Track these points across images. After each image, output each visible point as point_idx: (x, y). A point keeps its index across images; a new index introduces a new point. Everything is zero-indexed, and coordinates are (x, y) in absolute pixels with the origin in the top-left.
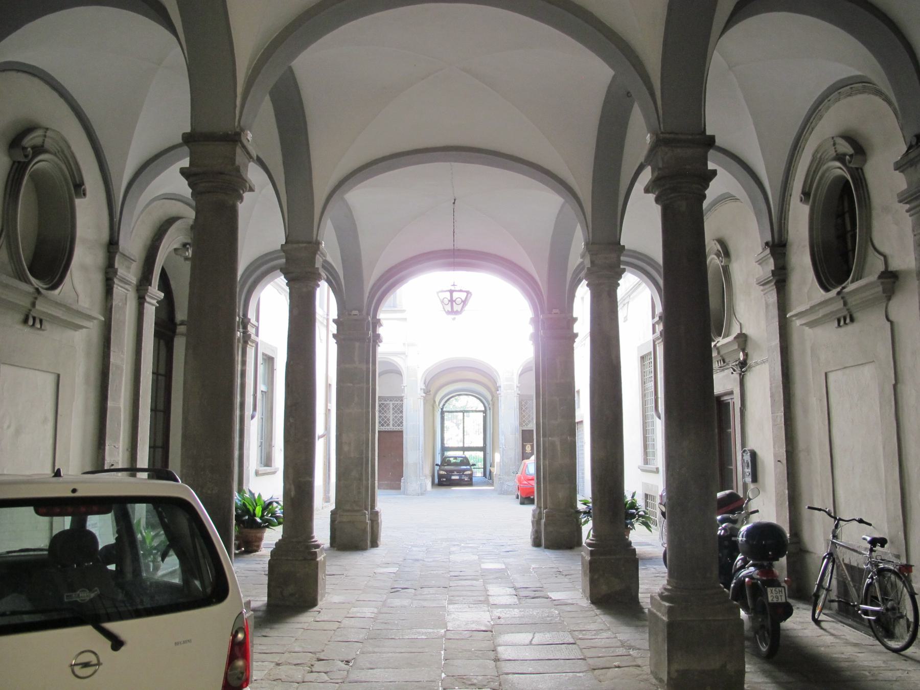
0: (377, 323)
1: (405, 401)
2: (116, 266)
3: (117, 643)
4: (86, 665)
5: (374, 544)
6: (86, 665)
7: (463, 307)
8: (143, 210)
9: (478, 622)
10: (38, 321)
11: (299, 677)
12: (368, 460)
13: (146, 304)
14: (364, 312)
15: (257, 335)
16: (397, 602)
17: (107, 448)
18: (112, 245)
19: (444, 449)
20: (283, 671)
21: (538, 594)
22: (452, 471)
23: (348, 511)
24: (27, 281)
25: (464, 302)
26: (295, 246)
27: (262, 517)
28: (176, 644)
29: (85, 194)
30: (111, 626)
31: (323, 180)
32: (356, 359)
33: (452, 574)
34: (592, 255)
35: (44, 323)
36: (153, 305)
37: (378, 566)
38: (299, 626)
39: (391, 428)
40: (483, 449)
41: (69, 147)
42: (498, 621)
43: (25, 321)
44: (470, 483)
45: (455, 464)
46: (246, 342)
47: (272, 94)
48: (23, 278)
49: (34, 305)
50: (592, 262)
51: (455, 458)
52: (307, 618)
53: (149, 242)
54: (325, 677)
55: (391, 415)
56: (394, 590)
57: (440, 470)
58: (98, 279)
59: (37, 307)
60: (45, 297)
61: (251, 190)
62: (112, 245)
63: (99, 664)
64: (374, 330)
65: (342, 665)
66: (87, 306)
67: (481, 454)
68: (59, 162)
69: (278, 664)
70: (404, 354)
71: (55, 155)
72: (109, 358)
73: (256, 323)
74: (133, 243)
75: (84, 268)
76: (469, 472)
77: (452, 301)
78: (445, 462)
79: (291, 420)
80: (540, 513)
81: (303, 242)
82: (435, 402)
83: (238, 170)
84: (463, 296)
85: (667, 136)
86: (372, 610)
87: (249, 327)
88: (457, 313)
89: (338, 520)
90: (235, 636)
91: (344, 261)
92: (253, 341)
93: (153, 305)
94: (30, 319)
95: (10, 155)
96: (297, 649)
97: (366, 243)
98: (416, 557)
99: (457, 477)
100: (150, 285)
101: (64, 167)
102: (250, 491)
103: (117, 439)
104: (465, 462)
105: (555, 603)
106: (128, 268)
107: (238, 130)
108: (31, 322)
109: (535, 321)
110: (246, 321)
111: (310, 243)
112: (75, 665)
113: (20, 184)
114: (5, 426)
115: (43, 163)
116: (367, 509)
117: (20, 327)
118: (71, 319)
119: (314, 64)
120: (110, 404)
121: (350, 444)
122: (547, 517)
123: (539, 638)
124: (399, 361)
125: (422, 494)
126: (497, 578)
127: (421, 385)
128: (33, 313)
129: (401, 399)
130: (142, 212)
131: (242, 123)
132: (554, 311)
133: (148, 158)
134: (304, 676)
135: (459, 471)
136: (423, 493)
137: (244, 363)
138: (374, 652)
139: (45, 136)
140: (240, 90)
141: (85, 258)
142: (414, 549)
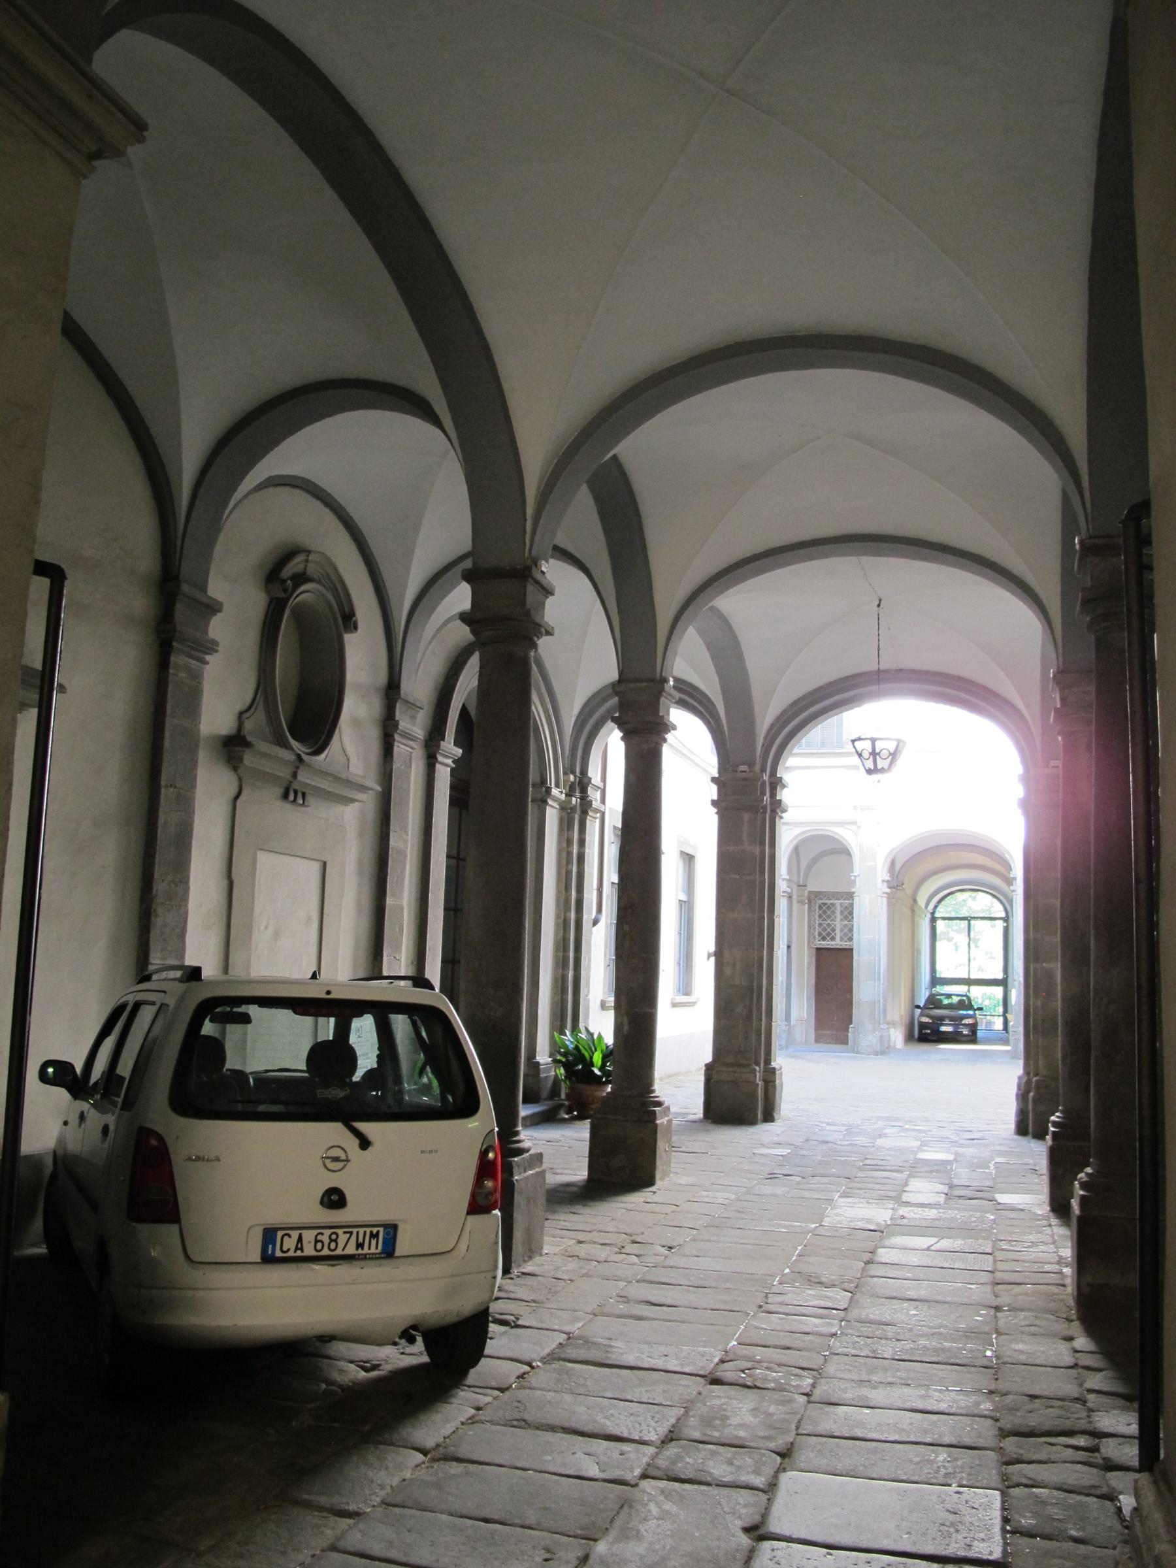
0: (776, 783)
1: (856, 900)
2: (398, 716)
3: (365, 1143)
4: (336, 1159)
5: (769, 1117)
6: (336, 1159)
7: (890, 765)
8: (433, 638)
9: (869, 1221)
10: (300, 795)
11: (603, 1257)
12: (760, 989)
13: (438, 766)
14: (757, 767)
15: (603, 801)
16: (768, 1189)
17: (385, 959)
18: (392, 690)
19: (935, 981)
20: (582, 1251)
21: (979, 1194)
22: (940, 1020)
23: (731, 1065)
24: (288, 747)
25: (894, 756)
26: (632, 685)
27: (602, 1068)
28: (423, 1152)
29: (356, 628)
30: (362, 1126)
31: (669, 587)
32: (745, 838)
33: (868, 1162)
34: (1062, 689)
35: (308, 797)
36: (447, 765)
37: (763, 1145)
38: (622, 1205)
39: (837, 943)
40: (1003, 983)
41: (336, 569)
42: (898, 1222)
43: (285, 796)
44: (972, 1038)
45: (950, 1007)
46: (584, 813)
47: (591, 484)
48: (282, 743)
49: (295, 775)
50: (1063, 700)
51: (949, 996)
52: (635, 1199)
53: (441, 680)
54: (635, 1259)
55: (838, 923)
56: (772, 1176)
57: (922, 1015)
58: (373, 735)
59: (299, 778)
60: (309, 766)
61: (549, 633)
62: (392, 690)
63: (348, 1161)
64: (773, 795)
65: (664, 1251)
66: (360, 772)
67: (998, 991)
68: (325, 592)
69: (580, 1242)
70: (855, 823)
71: (319, 582)
72: (388, 839)
73: (601, 785)
74: (419, 684)
75: (356, 723)
76: (969, 1021)
77: (874, 754)
78: (933, 1002)
79: (626, 928)
80: (1028, 1082)
81: (643, 681)
82: (915, 901)
83: (528, 614)
84: (891, 747)
85: (1096, 541)
86: (726, 1195)
87: (590, 791)
88: (882, 770)
89: (715, 1077)
90: (484, 1154)
91: (725, 691)
92: (597, 811)
93: (447, 765)
94: (291, 793)
95: (268, 592)
96: (609, 1229)
97: (756, 664)
98: (825, 1139)
99: (950, 1029)
100: (443, 739)
101: (331, 599)
102: (587, 1030)
103: (398, 948)
104: (966, 1004)
105: (999, 1207)
106: (413, 718)
107: (529, 563)
108: (291, 797)
109: (1025, 779)
110: (585, 780)
111: (653, 680)
112: (327, 1158)
113: (282, 616)
114: (262, 928)
115: (306, 594)
116: (757, 1064)
117: (279, 803)
118: (340, 790)
119: (643, 449)
120: (389, 901)
121: (734, 965)
122: (1038, 1087)
123: (945, 1243)
124: (847, 836)
125: (883, 1053)
126: (932, 1171)
127: (882, 874)
128: (295, 786)
129: (850, 896)
130: (430, 642)
131: (534, 553)
132: (1053, 763)
133: (436, 571)
134: (608, 1256)
135: (952, 1018)
136: (885, 1050)
137: (582, 843)
138: (709, 1241)
139: (307, 561)
140: (530, 511)
141: (358, 709)
142: (828, 1127)
